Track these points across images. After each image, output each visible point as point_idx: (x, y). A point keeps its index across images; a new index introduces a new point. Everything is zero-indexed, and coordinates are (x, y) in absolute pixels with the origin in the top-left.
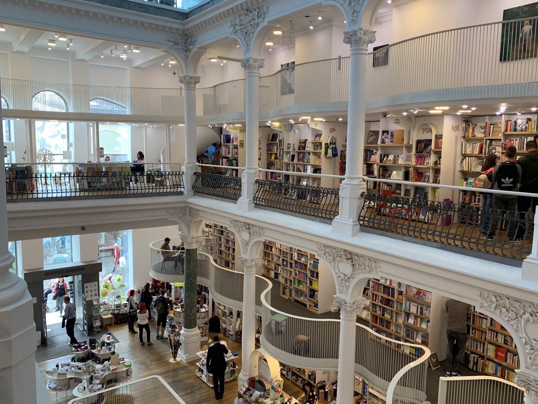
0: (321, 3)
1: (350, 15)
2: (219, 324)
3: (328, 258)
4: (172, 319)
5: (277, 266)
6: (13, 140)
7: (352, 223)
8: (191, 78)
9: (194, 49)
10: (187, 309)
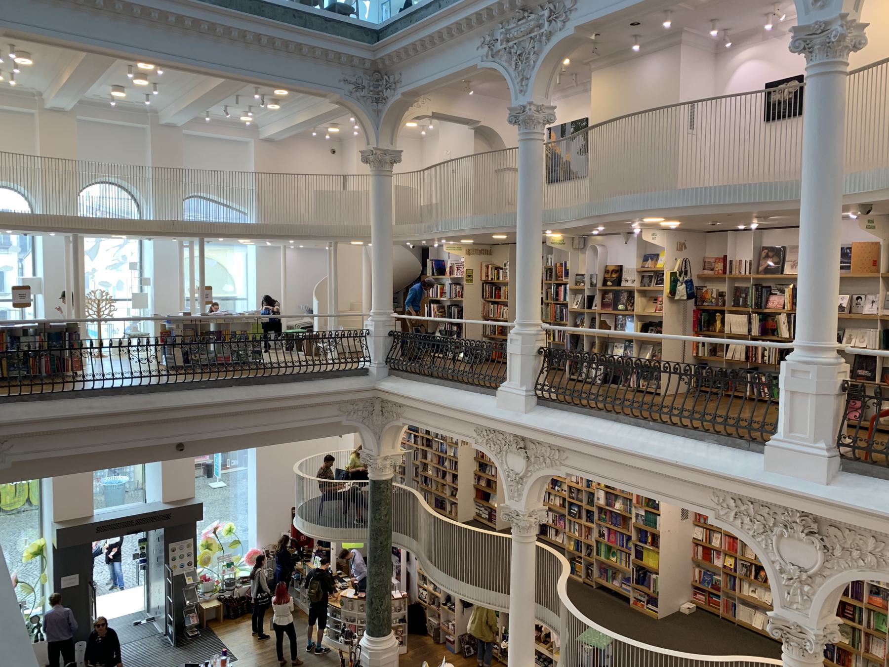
0: (476, 65)
1: (518, 83)
2: (424, 619)
3: (492, 449)
4: (336, 612)
6: (40, 274)
7: (825, 453)
8: (385, 152)
9: (394, 97)
10: (375, 597)
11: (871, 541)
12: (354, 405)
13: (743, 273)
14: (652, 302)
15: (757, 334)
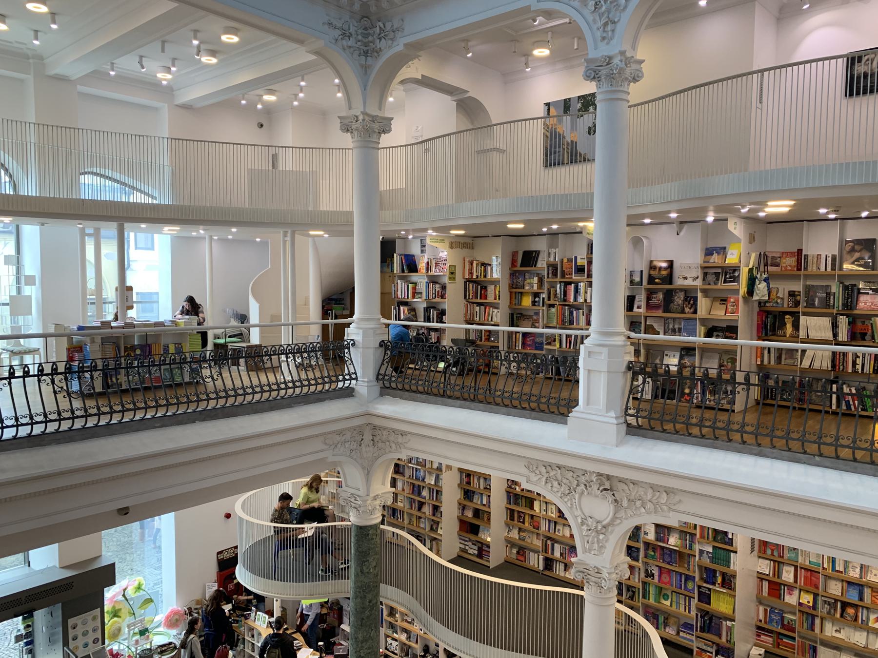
5: (549, 542)
8: (374, 119)
11: (650, 491)
12: (341, 435)
13: (823, 269)
14: (719, 302)
15: (845, 339)
